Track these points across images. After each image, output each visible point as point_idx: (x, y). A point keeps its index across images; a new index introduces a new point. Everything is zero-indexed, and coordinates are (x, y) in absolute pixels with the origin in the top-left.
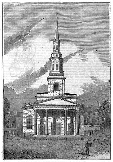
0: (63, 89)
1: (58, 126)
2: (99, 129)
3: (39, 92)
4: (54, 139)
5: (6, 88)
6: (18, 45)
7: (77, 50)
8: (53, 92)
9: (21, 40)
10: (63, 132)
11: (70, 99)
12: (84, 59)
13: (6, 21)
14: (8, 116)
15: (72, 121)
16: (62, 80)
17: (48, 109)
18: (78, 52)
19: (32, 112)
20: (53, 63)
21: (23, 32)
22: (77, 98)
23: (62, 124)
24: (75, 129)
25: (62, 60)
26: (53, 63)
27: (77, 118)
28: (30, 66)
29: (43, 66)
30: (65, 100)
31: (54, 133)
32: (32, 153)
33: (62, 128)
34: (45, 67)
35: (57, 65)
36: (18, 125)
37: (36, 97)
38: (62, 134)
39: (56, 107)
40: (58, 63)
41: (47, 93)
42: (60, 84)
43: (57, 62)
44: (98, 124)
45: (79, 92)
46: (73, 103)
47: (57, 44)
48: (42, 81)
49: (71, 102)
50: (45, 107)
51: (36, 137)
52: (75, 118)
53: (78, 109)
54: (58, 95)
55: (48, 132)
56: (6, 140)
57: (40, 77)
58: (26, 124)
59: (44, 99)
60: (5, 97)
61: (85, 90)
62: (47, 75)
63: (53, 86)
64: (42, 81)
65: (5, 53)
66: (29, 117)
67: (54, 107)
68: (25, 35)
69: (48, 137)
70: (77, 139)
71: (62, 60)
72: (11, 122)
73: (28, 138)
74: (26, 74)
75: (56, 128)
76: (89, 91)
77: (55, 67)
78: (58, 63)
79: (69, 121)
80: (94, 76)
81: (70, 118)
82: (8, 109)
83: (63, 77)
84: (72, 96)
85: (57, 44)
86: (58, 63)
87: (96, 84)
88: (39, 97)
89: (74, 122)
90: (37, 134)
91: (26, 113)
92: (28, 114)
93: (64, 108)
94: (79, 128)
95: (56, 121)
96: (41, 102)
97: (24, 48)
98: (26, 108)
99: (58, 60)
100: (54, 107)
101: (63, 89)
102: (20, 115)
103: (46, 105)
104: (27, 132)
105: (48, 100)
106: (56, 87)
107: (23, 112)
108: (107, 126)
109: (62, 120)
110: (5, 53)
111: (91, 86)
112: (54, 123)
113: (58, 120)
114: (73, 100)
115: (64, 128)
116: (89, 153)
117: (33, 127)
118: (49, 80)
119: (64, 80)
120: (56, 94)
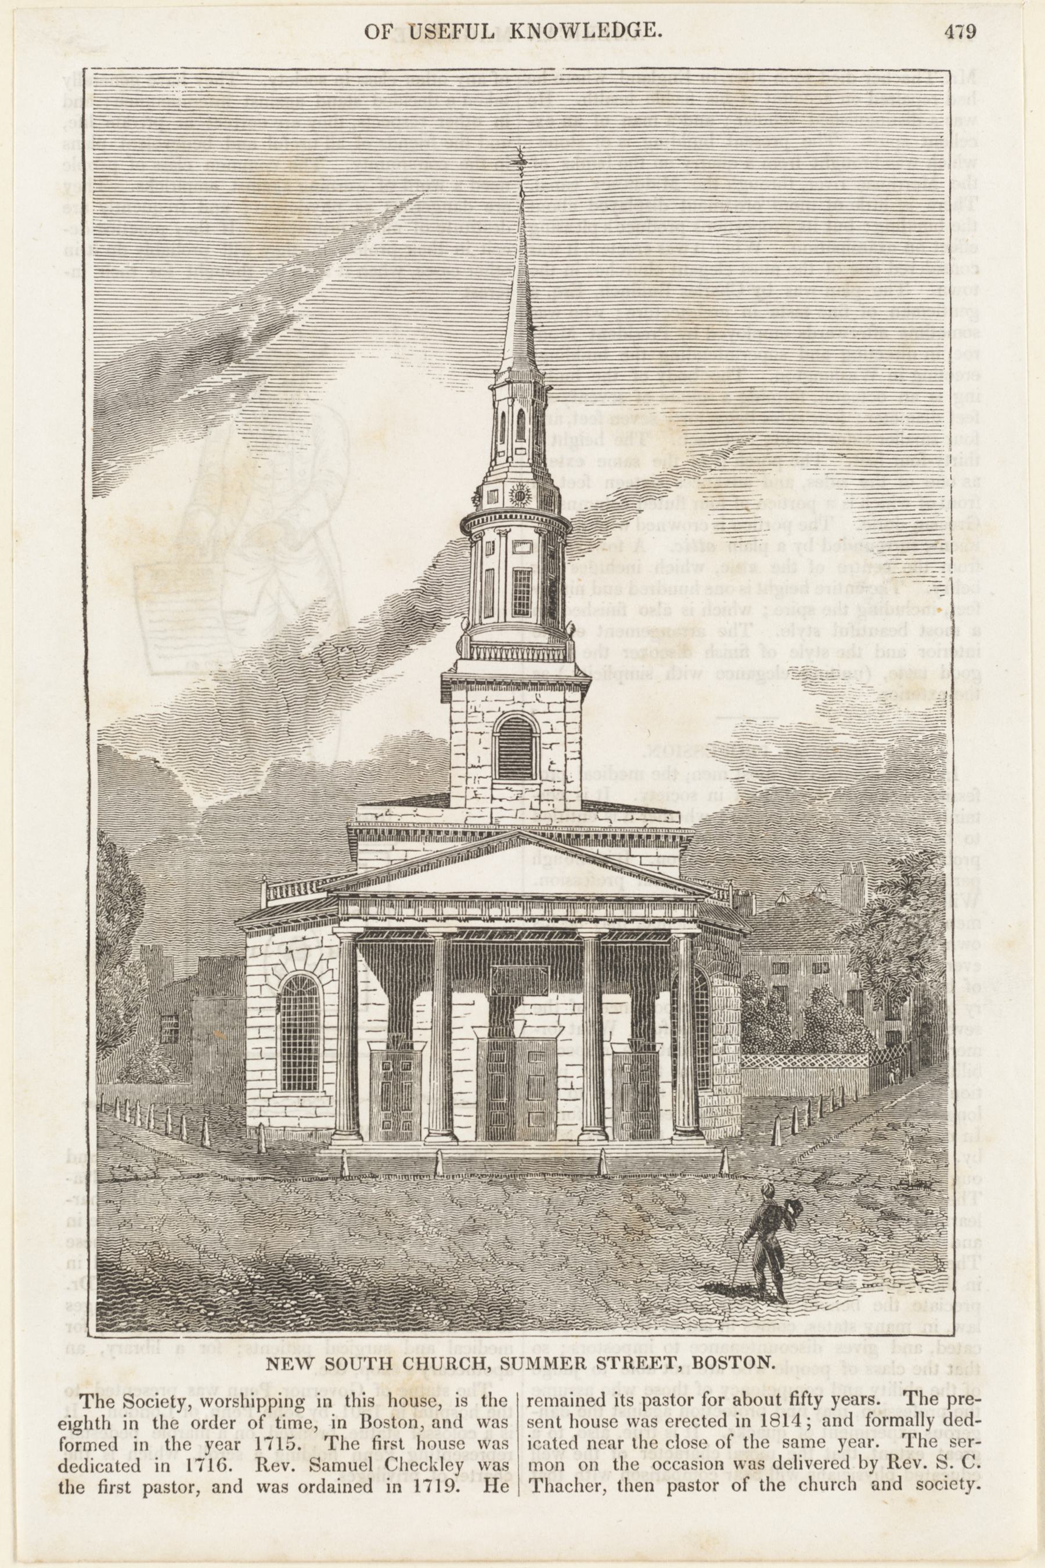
0: (573, 766)
1: (524, 1068)
2: (864, 1091)
3: (372, 790)
4: (512, 1174)
5: (112, 767)
6: (205, 412)
7: (680, 456)
8: (487, 793)
9: (232, 373)
10: (573, 1113)
11: (624, 851)
12: (739, 526)
13: (113, 217)
14: (127, 991)
15: (643, 1018)
16: (558, 696)
17: (452, 926)
18: (694, 468)
19: (319, 951)
20: (490, 562)
21: (249, 304)
22: (683, 842)
23: (562, 1047)
24: (665, 1088)
25: (557, 536)
26: (490, 562)
27: (683, 997)
28: (303, 586)
29: (405, 580)
30: (593, 860)
31: (497, 1123)
32: (321, 1282)
33: (562, 1083)
34: (422, 593)
35: (521, 576)
36: (208, 1062)
37: (355, 836)
38: (562, 1132)
39: (537, 912)
40: (532, 561)
41: (443, 801)
42: (545, 728)
43: (520, 550)
44: (855, 1048)
45: (703, 795)
46: (656, 880)
47: (517, 406)
48: (395, 707)
49: (640, 875)
50: (428, 911)
51: (355, 1152)
52: (664, 1000)
53: (693, 928)
54: (528, 819)
55: (449, 1122)
56: (114, 1177)
57: (390, 671)
58: (271, 1032)
59: (417, 849)
60: (101, 835)
61: (749, 777)
62: (439, 652)
63: (487, 740)
64: (395, 707)
65: (98, 481)
66: (298, 992)
67: (495, 912)
68: (260, 338)
69: (452, 1151)
70: (680, 1167)
71: (557, 536)
72: (156, 1022)
73: (288, 1162)
74: (274, 648)
75: (509, 1085)
76: (783, 793)
77: (503, 595)
78: (534, 544)
79: (619, 1026)
80: (824, 665)
81: (627, 998)
82: (129, 931)
83: (566, 670)
84: (637, 822)
85: (517, 406)
86: (534, 544)
87: (837, 729)
88: (378, 836)
89: (663, 1038)
90: (364, 1130)
91: (269, 962)
92: (290, 967)
93: (580, 920)
94: (702, 1079)
95: (518, 1027)
96: (389, 875)
97: (262, 440)
98: (272, 920)
99: (530, 534)
100: (495, 912)
101: (573, 766)
102: (224, 973)
103: (431, 898)
104: (276, 1112)
105: (452, 858)
106: (516, 751)
107: (250, 952)
108: (926, 1062)
109: (565, 1020)
110: (98, 481)
111: (799, 745)
112: (501, 1045)
113: (531, 1020)
114: (647, 856)
115: (578, 1083)
116: (779, 1279)
117: (330, 1044)
118: (458, 695)
119: (577, 696)
120: (514, 804)
